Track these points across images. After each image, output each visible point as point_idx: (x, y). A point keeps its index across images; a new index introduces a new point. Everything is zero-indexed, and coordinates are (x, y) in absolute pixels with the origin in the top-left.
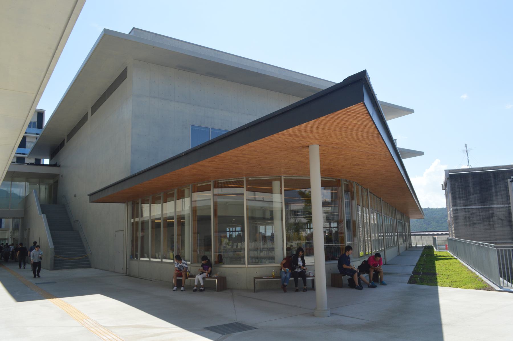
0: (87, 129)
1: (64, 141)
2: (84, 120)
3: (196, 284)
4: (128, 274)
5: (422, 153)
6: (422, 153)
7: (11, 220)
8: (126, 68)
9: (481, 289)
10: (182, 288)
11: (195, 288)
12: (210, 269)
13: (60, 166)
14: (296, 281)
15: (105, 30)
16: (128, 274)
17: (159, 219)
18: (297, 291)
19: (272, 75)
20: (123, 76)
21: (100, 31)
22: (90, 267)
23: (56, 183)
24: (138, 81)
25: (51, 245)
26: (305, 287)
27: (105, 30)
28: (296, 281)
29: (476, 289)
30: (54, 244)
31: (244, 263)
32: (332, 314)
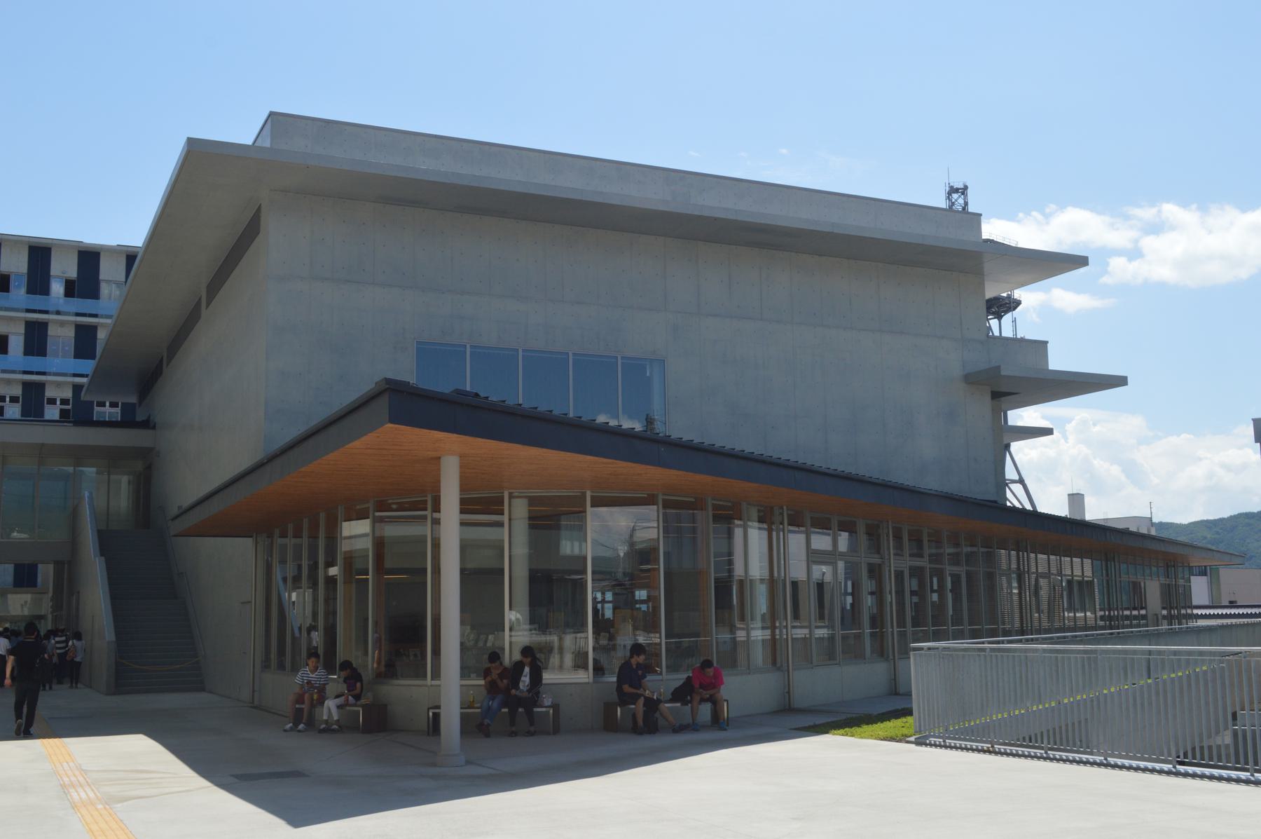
0: (202, 343)
1: (161, 361)
2: (191, 320)
3: (325, 717)
4: (256, 703)
5: (1121, 381)
6: (1121, 381)
7: (51, 567)
8: (259, 209)
9: (900, 741)
10: (301, 726)
11: (323, 726)
12: (358, 685)
13: (154, 428)
14: (513, 713)
15: (191, 142)
16: (256, 703)
17: (790, 531)
18: (513, 734)
19: (625, 204)
20: (251, 231)
21: (185, 140)
22: (203, 690)
23: (149, 468)
24: (281, 242)
25: (110, 635)
26: (532, 729)
27: (191, 142)
28: (513, 713)
29: (892, 739)
30: (117, 633)
31: (425, 676)
32: (468, 762)
